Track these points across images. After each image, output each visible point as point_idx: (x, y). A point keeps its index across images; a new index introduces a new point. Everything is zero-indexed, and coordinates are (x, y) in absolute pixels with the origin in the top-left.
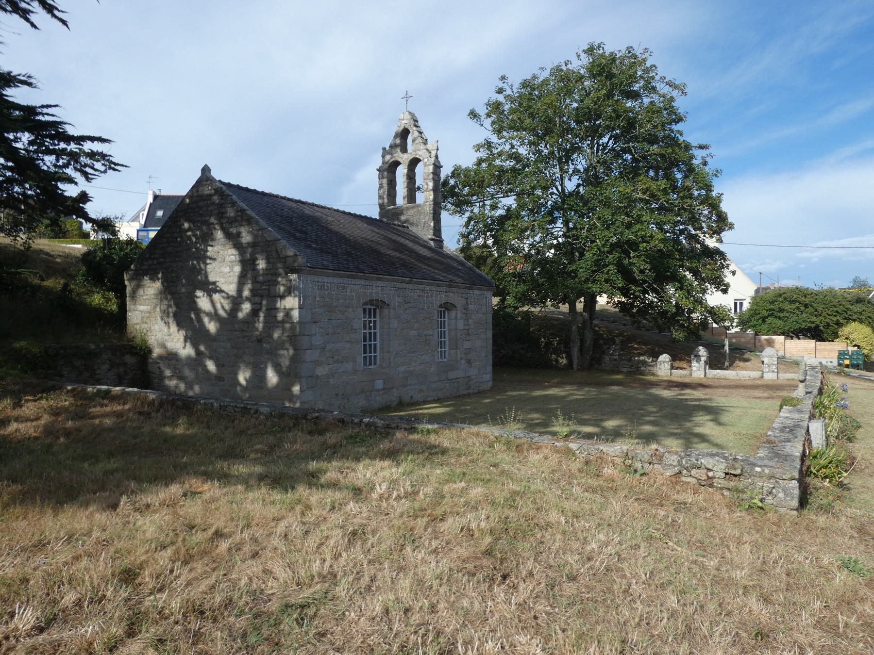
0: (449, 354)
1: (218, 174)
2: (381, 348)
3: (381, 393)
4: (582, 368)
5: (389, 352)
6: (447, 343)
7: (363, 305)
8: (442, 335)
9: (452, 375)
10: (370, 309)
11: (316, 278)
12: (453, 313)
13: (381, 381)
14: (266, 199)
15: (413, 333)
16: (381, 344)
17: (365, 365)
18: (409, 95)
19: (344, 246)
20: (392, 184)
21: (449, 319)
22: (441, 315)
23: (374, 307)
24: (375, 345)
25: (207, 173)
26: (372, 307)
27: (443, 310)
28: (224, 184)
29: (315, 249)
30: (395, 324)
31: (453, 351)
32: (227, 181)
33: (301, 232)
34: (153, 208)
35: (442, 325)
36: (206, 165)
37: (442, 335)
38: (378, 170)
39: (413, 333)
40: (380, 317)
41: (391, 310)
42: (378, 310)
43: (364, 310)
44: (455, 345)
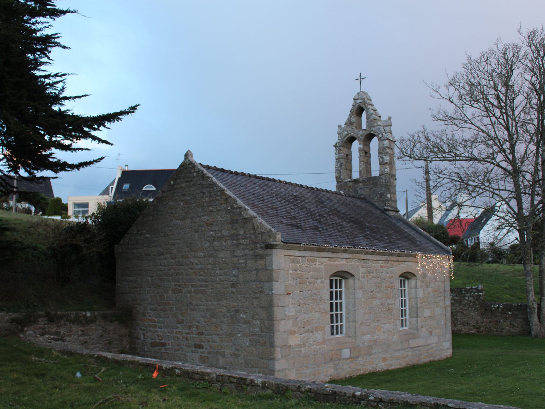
0: (410, 322)
1: (198, 159)
2: (347, 318)
3: (348, 361)
4: (74, 211)
5: (355, 321)
6: (407, 311)
7: (331, 276)
8: (403, 303)
9: (414, 343)
10: (336, 280)
11: (291, 252)
12: (413, 282)
13: (348, 350)
14: (239, 178)
15: (376, 302)
16: (347, 314)
17: (332, 334)
18: (358, 81)
19: (311, 220)
20: (348, 157)
21: (409, 287)
22: (402, 284)
23: (340, 277)
24: (341, 314)
25: (190, 158)
26: (338, 278)
27: (403, 279)
28: (203, 166)
29: (287, 225)
30: (360, 294)
31: (414, 320)
32: (205, 164)
33: (272, 208)
34: (121, 181)
35: (403, 293)
36: (189, 151)
37: (403, 303)
38: (335, 146)
39: (376, 302)
40: (346, 287)
41: (357, 281)
42: (343, 281)
43: (331, 281)
44: (415, 313)
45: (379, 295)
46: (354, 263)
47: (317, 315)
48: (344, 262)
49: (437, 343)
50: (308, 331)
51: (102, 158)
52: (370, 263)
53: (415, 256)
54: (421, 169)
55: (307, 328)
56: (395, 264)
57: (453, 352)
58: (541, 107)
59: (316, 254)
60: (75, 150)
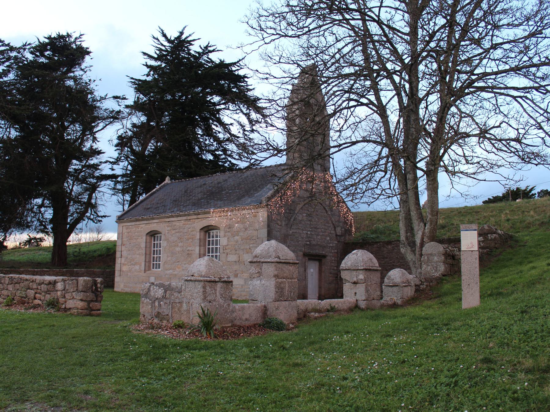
15: (178, 249)
45: (180, 244)
46: (162, 225)
47: (138, 256)
48: (155, 225)
49: (242, 286)
50: (132, 264)
51: (145, 54)
52: (174, 223)
53: (209, 213)
54: (476, 232)
55: (132, 262)
56: (197, 220)
57: (274, 239)
58: (435, 165)
59: (138, 223)
60: (162, 30)
